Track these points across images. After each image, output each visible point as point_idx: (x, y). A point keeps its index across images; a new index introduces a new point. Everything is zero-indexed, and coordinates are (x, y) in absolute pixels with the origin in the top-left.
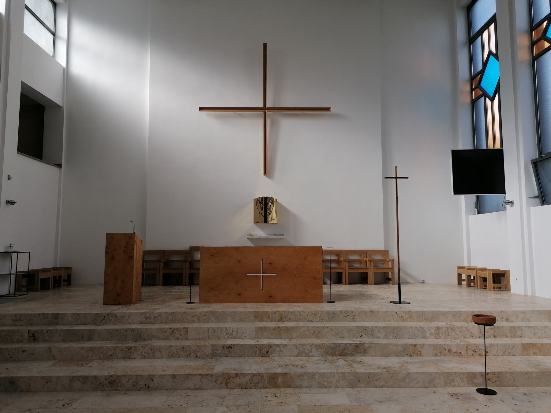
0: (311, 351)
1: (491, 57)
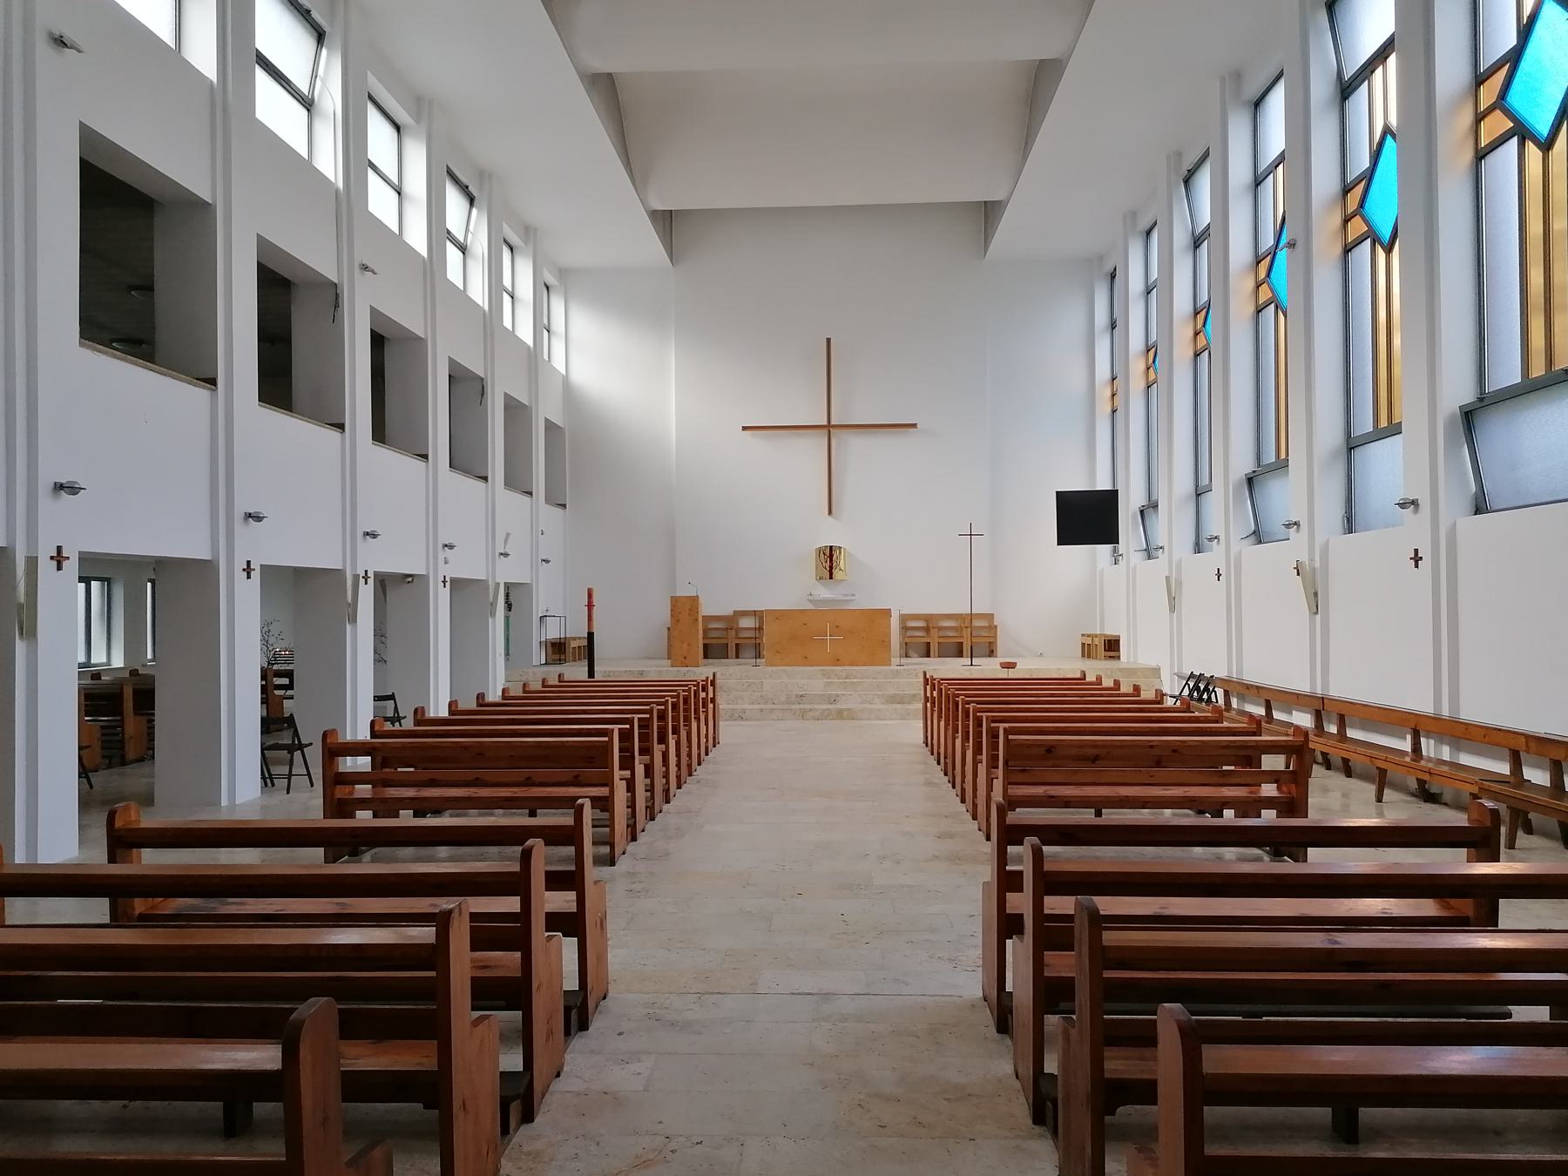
0: (873, 699)
1: (1389, 138)
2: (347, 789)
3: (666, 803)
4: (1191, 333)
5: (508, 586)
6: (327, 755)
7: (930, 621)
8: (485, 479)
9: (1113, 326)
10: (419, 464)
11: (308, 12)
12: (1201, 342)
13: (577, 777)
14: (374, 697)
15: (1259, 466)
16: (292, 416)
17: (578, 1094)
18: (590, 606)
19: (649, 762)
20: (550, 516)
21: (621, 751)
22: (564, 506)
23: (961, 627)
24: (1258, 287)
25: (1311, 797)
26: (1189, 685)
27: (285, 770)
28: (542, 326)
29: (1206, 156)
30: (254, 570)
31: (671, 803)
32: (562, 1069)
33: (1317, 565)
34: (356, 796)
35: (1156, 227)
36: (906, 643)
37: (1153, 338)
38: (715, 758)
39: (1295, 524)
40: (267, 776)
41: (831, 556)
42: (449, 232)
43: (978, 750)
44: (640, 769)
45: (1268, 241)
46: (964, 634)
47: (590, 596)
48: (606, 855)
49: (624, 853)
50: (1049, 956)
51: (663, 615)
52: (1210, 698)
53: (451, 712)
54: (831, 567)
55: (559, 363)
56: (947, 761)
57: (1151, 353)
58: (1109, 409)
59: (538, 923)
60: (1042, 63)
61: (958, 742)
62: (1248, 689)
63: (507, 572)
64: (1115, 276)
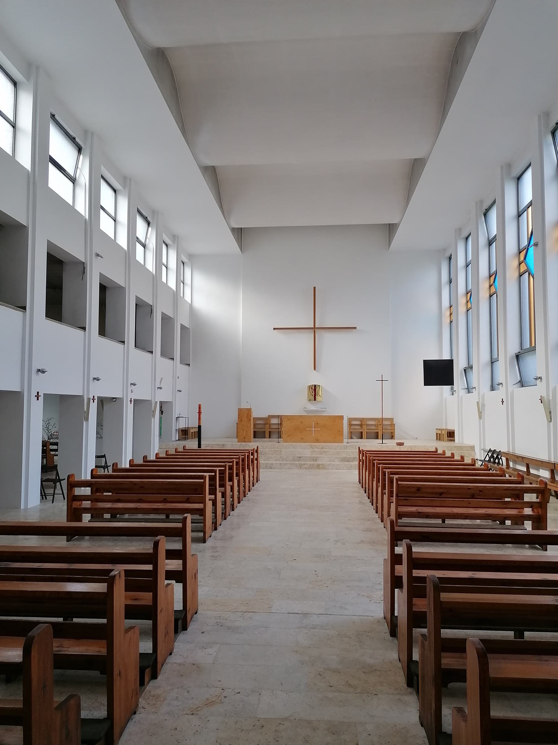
2: (79, 503)
3: (232, 511)
4: (488, 286)
5: (161, 403)
6: (69, 487)
7: (362, 422)
8: (152, 352)
9: (450, 282)
10: (121, 346)
11: (74, 138)
12: (493, 290)
13: (188, 499)
14: (96, 456)
15: (522, 349)
16: (61, 324)
17: (180, 664)
18: (200, 413)
19: (224, 491)
20: (182, 369)
21: (210, 485)
22: (189, 365)
23: (377, 424)
24: (520, 264)
25: (549, 513)
26: (489, 455)
27: (51, 491)
28: (180, 281)
29: (494, 202)
30: (40, 396)
31: (235, 511)
32: (173, 650)
33: (551, 398)
34: (83, 506)
35: (471, 236)
36: (351, 432)
37: (470, 287)
38: (257, 488)
39: (540, 378)
40: (43, 494)
41: (315, 390)
42: (137, 238)
43: (384, 488)
44: (219, 495)
45: (524, 243)
46: (379, 428)
47: (200, 408)
48: (201, 537)
49: (210, 537)
50: (415, 601)
51: (234, 417)
52: (499, 462)
53: (130, 465)
54: (315, 395)
55: (188, 298)
56: (369, 491)
57: (469, 294)
58: (449, 321)
59: (161, 575)
60: (416, 160)
61: (375, 483)
62: (518, 458)
63: (161, 396)
64: (451, 258)
